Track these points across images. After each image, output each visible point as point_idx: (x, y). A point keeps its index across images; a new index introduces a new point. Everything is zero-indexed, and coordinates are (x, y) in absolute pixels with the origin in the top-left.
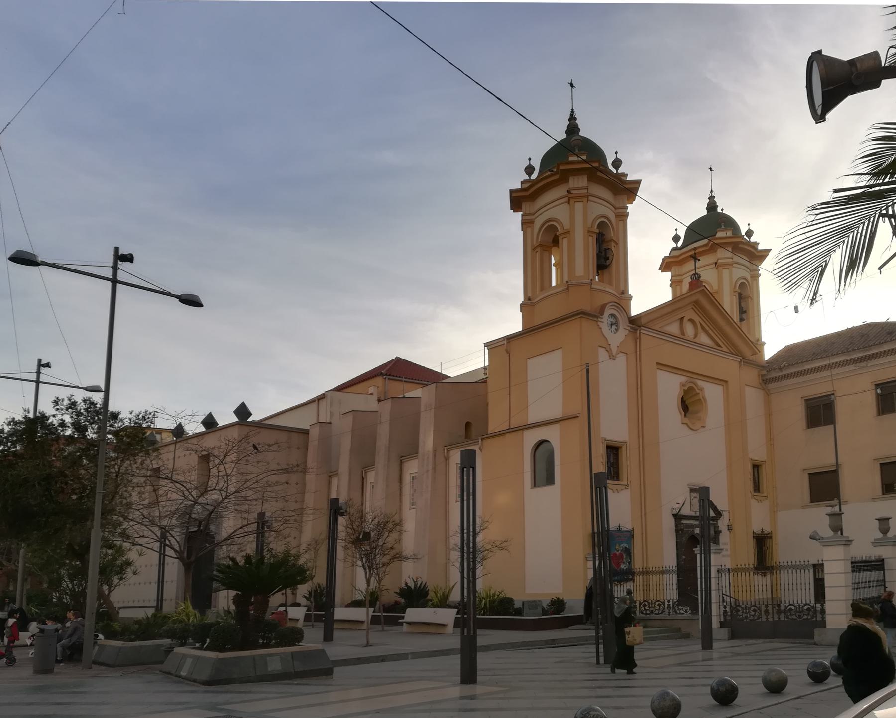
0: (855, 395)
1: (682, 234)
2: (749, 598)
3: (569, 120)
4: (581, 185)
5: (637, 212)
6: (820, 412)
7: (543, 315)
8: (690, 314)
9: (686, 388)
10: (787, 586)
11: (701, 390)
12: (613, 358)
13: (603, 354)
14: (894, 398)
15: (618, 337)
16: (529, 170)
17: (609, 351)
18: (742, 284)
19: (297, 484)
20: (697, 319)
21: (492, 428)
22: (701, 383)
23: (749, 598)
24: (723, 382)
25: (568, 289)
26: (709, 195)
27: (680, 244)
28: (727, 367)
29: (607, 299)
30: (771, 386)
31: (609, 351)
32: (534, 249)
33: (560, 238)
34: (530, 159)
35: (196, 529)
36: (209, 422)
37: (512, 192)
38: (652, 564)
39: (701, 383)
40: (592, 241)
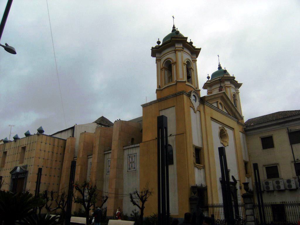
0: (281, 138)
1: (210, 76)
2: (295, 220)
3: (173, 28)
4: (180, 46)
5: (200, 60)
6: (268, 143)
7: (166, 93)
8: (220, 101)
9: (221, 129)
10: (269, 215)
11: (226, 130)
12: (195, 112)
13: (192, 111)
14: (296, 137)
15: (196, 104)
16: (159, 42)
17: (194, 109)
18: (234, 94)
19: (61, 154)
20: (222, 103)
21: (143, 141)
22: (226, 128)
23: (295, 220)
24: (233, 129)
25: (176, 84)
26: (218, 64)
27: (210, 79)
28: (232, 123)
29: (191, 89)
30: (249, 132)
31: (194, 109)
32: (161, 69)
33: (172, 65)
34: (159, 39)
35: (15, 178)
36: (27, 135)
37: (153, 48)
38: (215, 203)
39: (226, 128)
40: (185, 68)
